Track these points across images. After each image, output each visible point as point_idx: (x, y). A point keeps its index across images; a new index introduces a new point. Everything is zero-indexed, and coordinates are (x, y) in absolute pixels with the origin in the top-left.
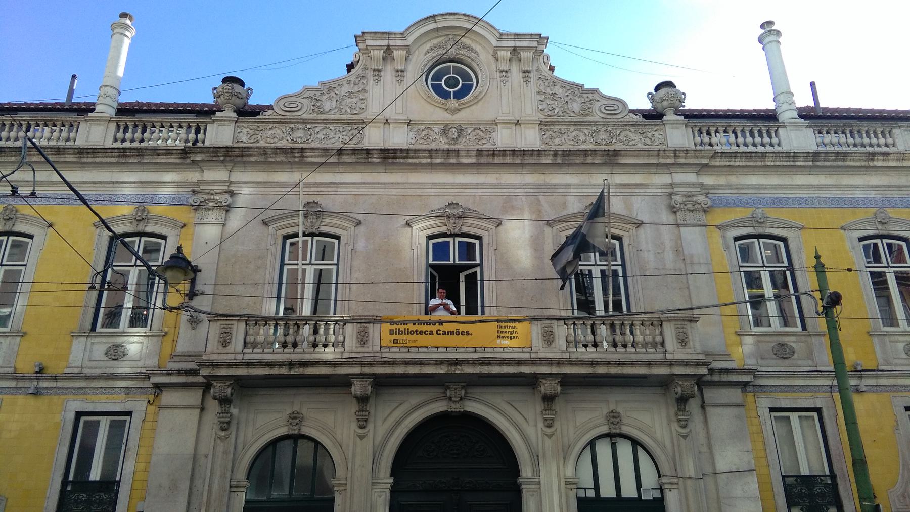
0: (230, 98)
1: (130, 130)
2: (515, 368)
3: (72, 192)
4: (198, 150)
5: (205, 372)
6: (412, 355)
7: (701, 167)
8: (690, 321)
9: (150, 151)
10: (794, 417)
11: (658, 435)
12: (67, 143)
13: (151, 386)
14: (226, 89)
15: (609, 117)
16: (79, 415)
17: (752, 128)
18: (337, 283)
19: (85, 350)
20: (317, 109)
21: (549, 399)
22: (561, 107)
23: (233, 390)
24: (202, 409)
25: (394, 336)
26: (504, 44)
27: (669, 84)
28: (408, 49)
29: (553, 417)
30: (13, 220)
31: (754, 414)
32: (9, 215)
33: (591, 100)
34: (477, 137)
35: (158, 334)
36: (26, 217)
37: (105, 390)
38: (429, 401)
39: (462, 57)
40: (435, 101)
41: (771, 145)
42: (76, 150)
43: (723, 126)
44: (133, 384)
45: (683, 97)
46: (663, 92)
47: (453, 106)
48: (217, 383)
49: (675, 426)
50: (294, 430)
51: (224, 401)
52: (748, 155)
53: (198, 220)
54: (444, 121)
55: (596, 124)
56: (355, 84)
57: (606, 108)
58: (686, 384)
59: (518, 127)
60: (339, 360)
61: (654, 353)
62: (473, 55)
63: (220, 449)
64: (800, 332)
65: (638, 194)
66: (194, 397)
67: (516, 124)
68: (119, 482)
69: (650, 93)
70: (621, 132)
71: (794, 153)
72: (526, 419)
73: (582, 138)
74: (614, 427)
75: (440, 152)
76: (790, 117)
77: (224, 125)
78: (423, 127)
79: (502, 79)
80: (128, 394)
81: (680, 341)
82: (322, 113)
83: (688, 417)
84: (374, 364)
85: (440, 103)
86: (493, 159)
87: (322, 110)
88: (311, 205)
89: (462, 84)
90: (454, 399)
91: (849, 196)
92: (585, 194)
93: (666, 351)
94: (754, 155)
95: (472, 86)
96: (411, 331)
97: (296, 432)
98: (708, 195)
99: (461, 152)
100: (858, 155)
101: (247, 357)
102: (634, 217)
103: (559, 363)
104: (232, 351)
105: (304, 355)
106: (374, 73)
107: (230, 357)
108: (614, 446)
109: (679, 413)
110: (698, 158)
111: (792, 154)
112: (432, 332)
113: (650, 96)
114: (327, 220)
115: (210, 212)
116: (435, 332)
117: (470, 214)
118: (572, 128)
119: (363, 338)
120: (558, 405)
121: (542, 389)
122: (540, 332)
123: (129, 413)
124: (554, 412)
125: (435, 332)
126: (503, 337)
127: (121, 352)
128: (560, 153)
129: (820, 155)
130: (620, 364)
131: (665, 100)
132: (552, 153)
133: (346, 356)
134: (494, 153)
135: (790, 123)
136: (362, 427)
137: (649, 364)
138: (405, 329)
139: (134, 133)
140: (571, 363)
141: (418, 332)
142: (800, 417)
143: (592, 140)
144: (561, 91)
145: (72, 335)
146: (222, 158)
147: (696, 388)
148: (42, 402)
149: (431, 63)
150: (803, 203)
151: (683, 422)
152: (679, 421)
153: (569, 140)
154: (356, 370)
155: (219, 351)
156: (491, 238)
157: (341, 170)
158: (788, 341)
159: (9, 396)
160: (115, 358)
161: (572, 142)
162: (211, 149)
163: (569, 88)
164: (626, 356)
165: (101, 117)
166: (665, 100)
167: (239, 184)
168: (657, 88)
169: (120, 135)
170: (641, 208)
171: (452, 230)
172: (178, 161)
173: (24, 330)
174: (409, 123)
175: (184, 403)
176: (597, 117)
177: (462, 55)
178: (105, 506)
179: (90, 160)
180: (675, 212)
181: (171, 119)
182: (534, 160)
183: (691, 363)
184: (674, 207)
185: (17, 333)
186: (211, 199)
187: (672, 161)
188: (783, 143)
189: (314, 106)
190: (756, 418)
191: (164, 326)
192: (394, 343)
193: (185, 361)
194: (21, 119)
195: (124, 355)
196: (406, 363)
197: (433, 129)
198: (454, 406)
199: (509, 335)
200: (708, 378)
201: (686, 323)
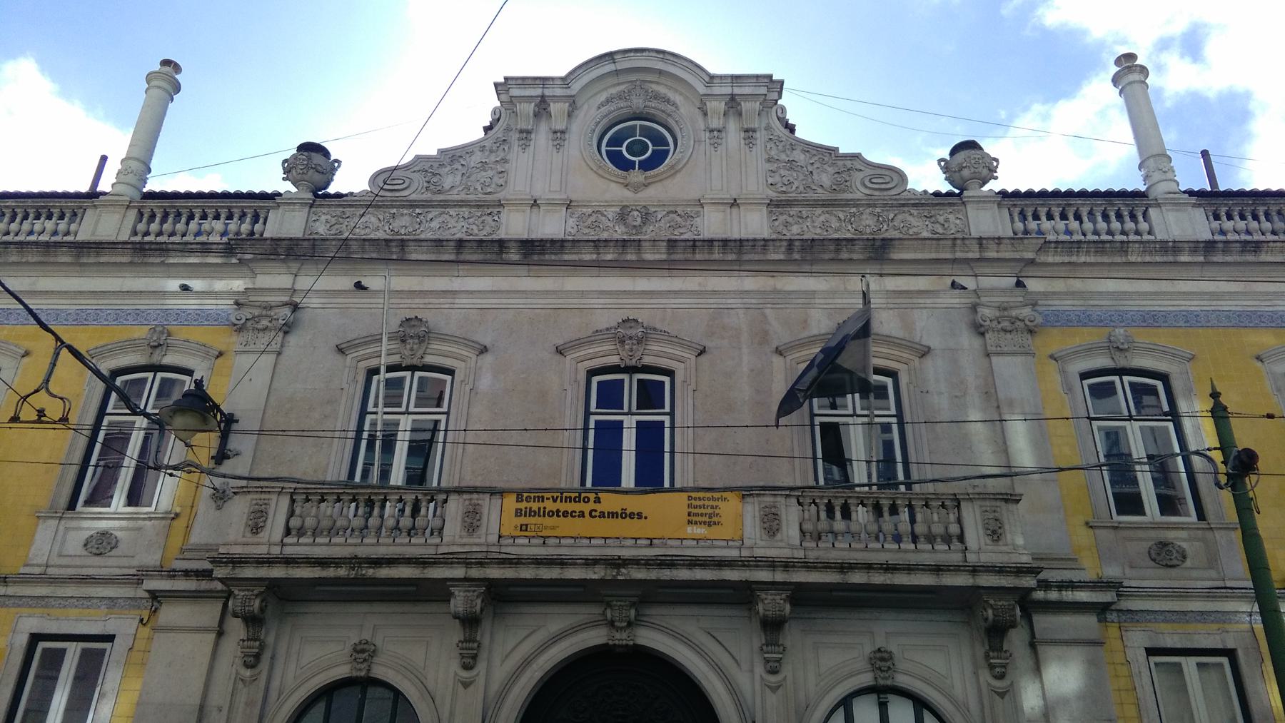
2: (714, 572)
3: (21, 307)
5: (220, 572)
6: (549, 549)
7: (1023, 264)
8: (1006, 501)
10: (1189, 664)
11: (958, 691)
12: (197, 238)
13: (147, 595)
15: (877, 193)
16: (35, 638)
17: (1105, 208)
18: (444, 442)
20: (432, 187)
21: (773, 626)
22: (803, 180)
23: (264, 604)
24: (220, 634)
25: (523, 520)
26: (717, 90)
27: (971, 145)
28: (573, 103)
29: (781, 656)
31: (1119, 658)
33: (849, 170)
34: (672, 224)
38: (579, 628)
39: (652, 111)
40: (610, 173)
41: (1138, 233)
43: (1059, 205)
45: (995, 164)
46: (961, 155)
47: (636, 180)
48: (239, 590)
49: (985, 676)
50: (360, 670)
51: (254, 621)
52: (1100, 247)
54: (622, 202)
55: (855, 203)
56: (491, 151)
57: (873, 181)
58: (1000, 603)
59: (735, 210)
60: (431, 556)
61: (945, 552)
62: (669, 108)
63: (242, 698)
64: (1194, 524)
65: (922, 306)
66: (209, 613)
67: (732, 205)
69: (942, 160)
70: (895, 215)
71: (1175, 242)
72: (736, 661)
73: (835, 224)
74: (882, 675)
75: (612, 244)
76: (1167, 190)
78: (590, 210)
79: (712, 141)
81: (989, 532)
82: (439, 192)
83: (1008, 661)
84: (487, 563)
85: (618, 176)
86: (694, 253)
87: (439, 188)
88: (413, 323)
89: (653, 151)
90: (617, 624)
91: (1267, 309)
92: (838, 306)
93: (966, 549)
94: (1108, 245)
95: (668, 151)
96: (549, 512)
97: (363, 674)
98: (1037, 308)
99: (643, 244)
100: (1278, 244)
101: (289, 551)
102: (917, 340)
103: (787, 565)
104: (265, 540)
105: (377, 548)
106: (521, 135)
107: (262, 550)
108: (883, 707)
109: (991, 654)
110: (1017, 251)
111: (1171, 244)
112: (583, 512)
113: (943, 164)
114: (435, 346)
116: (587, 514)
117: (655, 336)
118: (819, 211)
119: (472, 521)
120: (792, 636)
121: (760, 608)
122: (757, 514)
123: (110, 638)
124: (782, 648)
125: (587, 514)
126: (696, 523)
128: (797, 243)
129: (1216, 245)
130: (888, 568)
131: (965, 167)
132: (785, 244)
133: (443, 550)
134: (694, 244)
135: (1166, 199)
136: (467, 667)
137: (937, 569)
138: (539, 509)
139: (175, 222)
140: (807, 566)
141: (560, 514)
142: (1199, 665)
143: (850, 227)
144: (802, 157)
145: (38, 517)
147: (1018, 611)
149: (605, 121)
150: (1191, 320)
151: (998, 670)
152: (992, 667)
153: (814, 227)
154: (459, 572)
155: (245, 540)
156: (688, 372)
157: (461, 272)
158: (1175, 539)
161: (819, 231)
162: (268, 242)
163: (815, 152)
164: (901, 555)
165: (117, 201)
166: (965, 167)
168: (954, 151)
169: (141, 227)
170: (926, 327)
171: (627, 361)
174: (569, 205)
175: (193, 624)
176: (859, 193)
177: (653, 108)
179: (91, 260)
180: (983, 334)
181: (217, 202)
182: (756, 256)
183: (1009, 569)
184: (981, 326)
187: (977, 255)
188: (1156, 230)
189: (429, 182)
190: (1122, 664)
192: (521, 530)
196: (538, 562)
197: (605, 213)
198: (618, 636)
199: (707, 519)
200: (1039, 595)
201: (998, 503)
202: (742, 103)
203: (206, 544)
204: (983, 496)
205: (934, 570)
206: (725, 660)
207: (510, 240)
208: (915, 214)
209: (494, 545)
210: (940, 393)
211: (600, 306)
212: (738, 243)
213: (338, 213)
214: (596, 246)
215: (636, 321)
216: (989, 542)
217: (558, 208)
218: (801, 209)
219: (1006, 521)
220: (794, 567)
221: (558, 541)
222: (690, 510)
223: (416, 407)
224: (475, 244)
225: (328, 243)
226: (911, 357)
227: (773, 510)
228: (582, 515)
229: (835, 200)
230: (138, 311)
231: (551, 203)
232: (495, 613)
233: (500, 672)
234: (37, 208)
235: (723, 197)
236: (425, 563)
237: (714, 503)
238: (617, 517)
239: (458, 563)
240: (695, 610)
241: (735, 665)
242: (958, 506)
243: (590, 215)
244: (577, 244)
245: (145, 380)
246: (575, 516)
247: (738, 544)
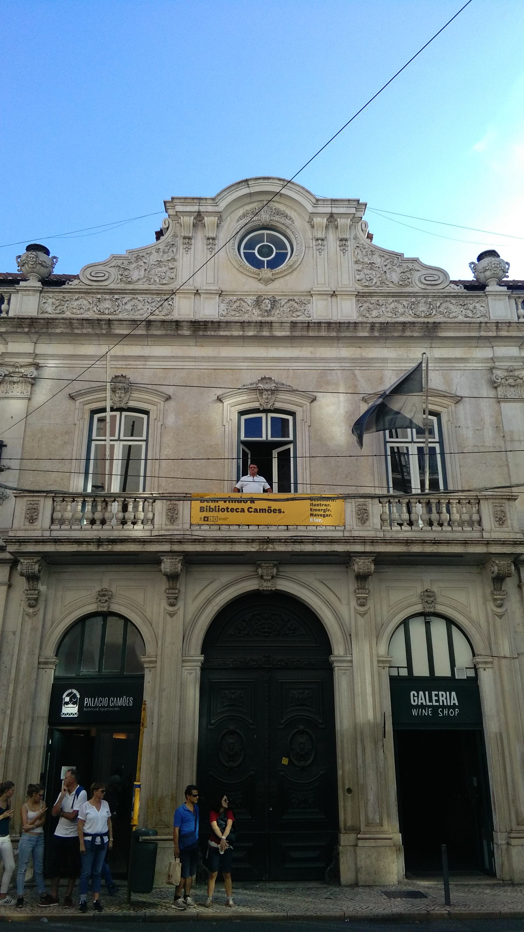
0: (35, 267)
2: (328, 546)
5: (11, 548)
8: (509, 499)
11: (474, 615)
14: (31, 257)
18: (146, 460)
20: (124, 279)
22: (379, 277)
24: (10, 586)
25: (205, 514)
26: (321, 210)
27: (492, 253)
28: (220, 215)
29: (367, 595)
34: (292, 308)
45: (507, 267)
46: (486, 261)
48: (24, 559)
49: (491, 606)
50: (104, 607)
51: (32, 578)
55: (414, 295)
57: (427, 278)
59: (334, 299)
61: (470, 532)
62: (288, 222)
65: (457, 368)
67: (332, 295)
69: (473, 263)
70: (441, 304)
73: (401, 310)
74: (428, 606)
75: (253, 324)
77: (28, 295)
78: (235, 298)
81: (497, 519)
82: (130, 283)
85: (253, 273)
86: (308, 332)
87: (129, 280)
88: (119, 379)
89: (276, 253)
93: (483, 530)
95: (287, 253)
97: (105, 609)
99: (274, 324)
101: (55, 534)
103: (373, 542)
107: (37, 534)
108: (428, 624)
113: (473, 266)
115: (15, 386)
116: (246, 510)
118: (391, 300)
121: (356, 567)
122: (354, 510)
124: (368, 591)
125: (246, 510)
126: (315, 515)
128: (377, 325)
132: (369, 325)
133: (155, 533)
134: (308, 325)
136: (172, 605)
137: (465, 543)
138: (215, 507)
140: (385, 542)
141: (229, 510)
143: (411, 312)
144: (379, 260)
146: (26, 330)
147: (513, 567)
152: (495, 600)
153: (387, 312)
154: (166, 548)
156: (305, 413)
161: (390, 315)
162: (16, 320)
163: (387, 257)
168: (480, 258)
174: (221, 294)
176: (417, 287)
180: (496, 388)
183: (509, 542)
184: (495, 382)
187: (494, 334)
189: (122, 275)
192: (204, 520)
196: (217, 541)
197: (246, 300)
198: (265, 584)
199: (322, 513)
201: (504, 501)
202: (338, 220)
204: (493, 497)
205: (463, 543)
206: (332, 598)
207: (183, 321)
208: (454, 303)
209: (188, 530)
210: (468, 427)
211: (245, 368)
212: (338, 324)
213: (60, 297)
214: (242, 326)
215: (270, 379)
216: (497, 525)
217: (214, 296)
218: (378, 299)
219: (507, 512)
220: (377, 542)
221: (228, 527)
222: (312, 507)
224: (159, 324)
225: (57, 321)
226: (450, 403)
227: (364, 506)
228: (243, 510)
229: (401, 293)
231: (209, 293)
232: (187, 571)
233: (192, 607)
235: (326, 289)
236: (144, 542)
237: (327, 503)
238: (265, 512)
239: (166, 542)
240: (314, 568)
241: (338, 601)
242: (479, 503)
243: (235, 302)
244: (229, 324)
246: (238, 512)
247: (342, 528)
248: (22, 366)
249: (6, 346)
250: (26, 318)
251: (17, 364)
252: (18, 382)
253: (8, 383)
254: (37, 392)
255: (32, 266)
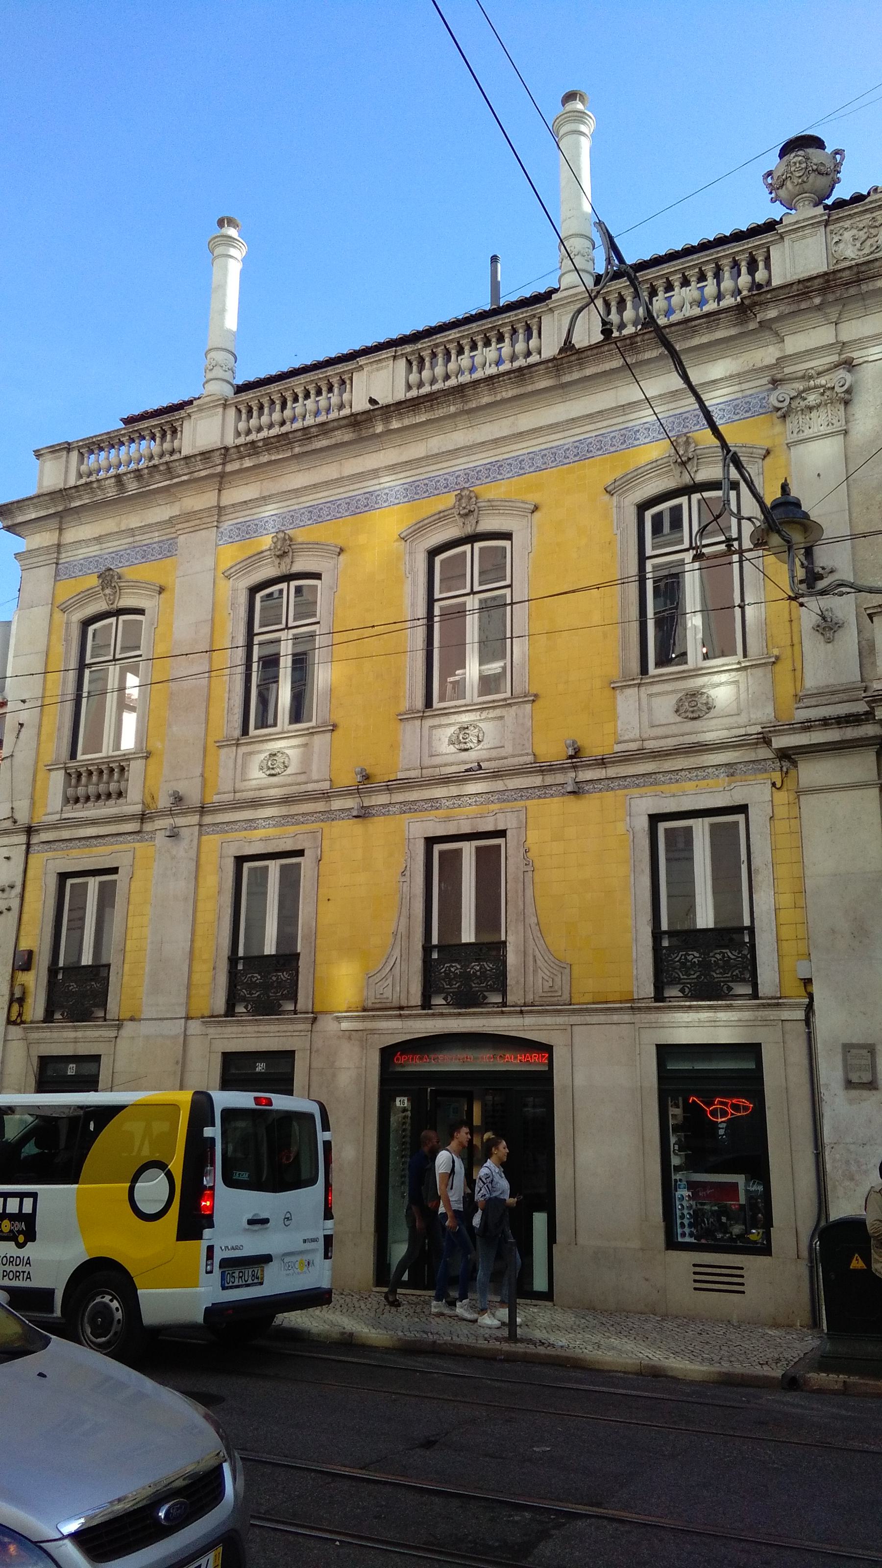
0: (805, 179)
1: (629, 304)
4: (769, 296)
9: (677, 328)
14: (795, 163)
19: (640, 708)
30: (476, 513)
32: (468, 507)
35: (763, 661)
36: (493, 504)
37: (690, 773)
42: (550, 364)
44: (737, 757)
53: (792, 436)
68: (751, 930)
77: (804, 237)
80: (732, 775)
115: (814, 414)
123: (742, 809)
127: (702, 704)
145: (613, 688)
146: (817, 301)
148: (589, 805)
159: (535, 801)
160: (695, 715)
162: (795, 287)
167: (861, 342)
172: (733, 332)
173: (533, 691)
175: (847, 780)
178: (737, 971)
179: (576, 376)
181: (698, 258)
185: (525, 696)
186: (809, 389)
191: (770, 646)
193: (826, 702)
194: (446, 339)
195: (709, 709)
203: (828, 686)
223: (480, 584)
230: (646, 426)
234: (484, 332)
245: (465, 553)
248: (819, 374)
249: (781, 345)
250: (816, 278)
251: (810, 371)
252: (818, 406)
253: (800, 412)
254: (856, 416)
255: (800, 180)
